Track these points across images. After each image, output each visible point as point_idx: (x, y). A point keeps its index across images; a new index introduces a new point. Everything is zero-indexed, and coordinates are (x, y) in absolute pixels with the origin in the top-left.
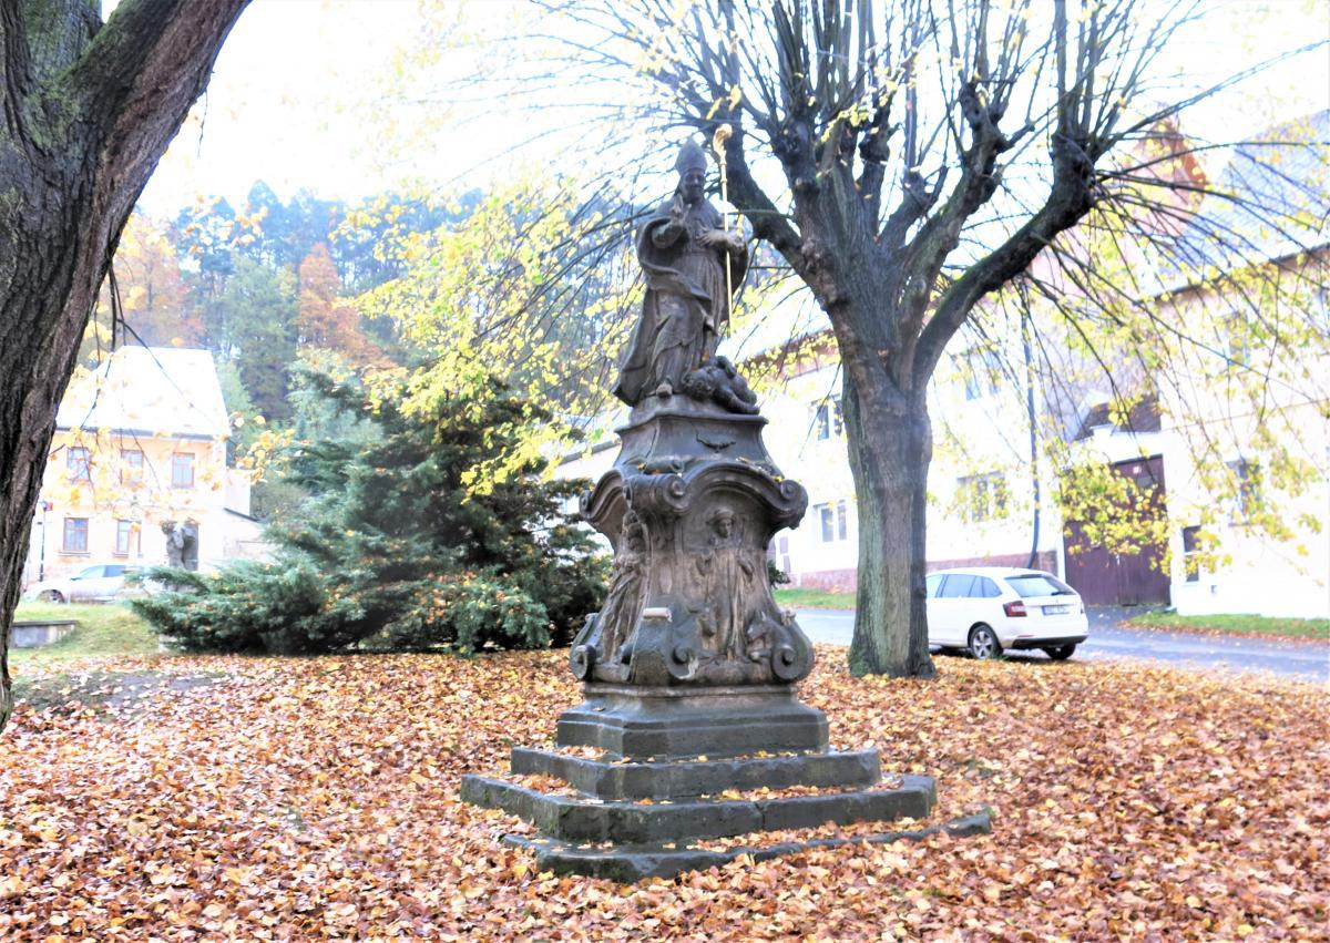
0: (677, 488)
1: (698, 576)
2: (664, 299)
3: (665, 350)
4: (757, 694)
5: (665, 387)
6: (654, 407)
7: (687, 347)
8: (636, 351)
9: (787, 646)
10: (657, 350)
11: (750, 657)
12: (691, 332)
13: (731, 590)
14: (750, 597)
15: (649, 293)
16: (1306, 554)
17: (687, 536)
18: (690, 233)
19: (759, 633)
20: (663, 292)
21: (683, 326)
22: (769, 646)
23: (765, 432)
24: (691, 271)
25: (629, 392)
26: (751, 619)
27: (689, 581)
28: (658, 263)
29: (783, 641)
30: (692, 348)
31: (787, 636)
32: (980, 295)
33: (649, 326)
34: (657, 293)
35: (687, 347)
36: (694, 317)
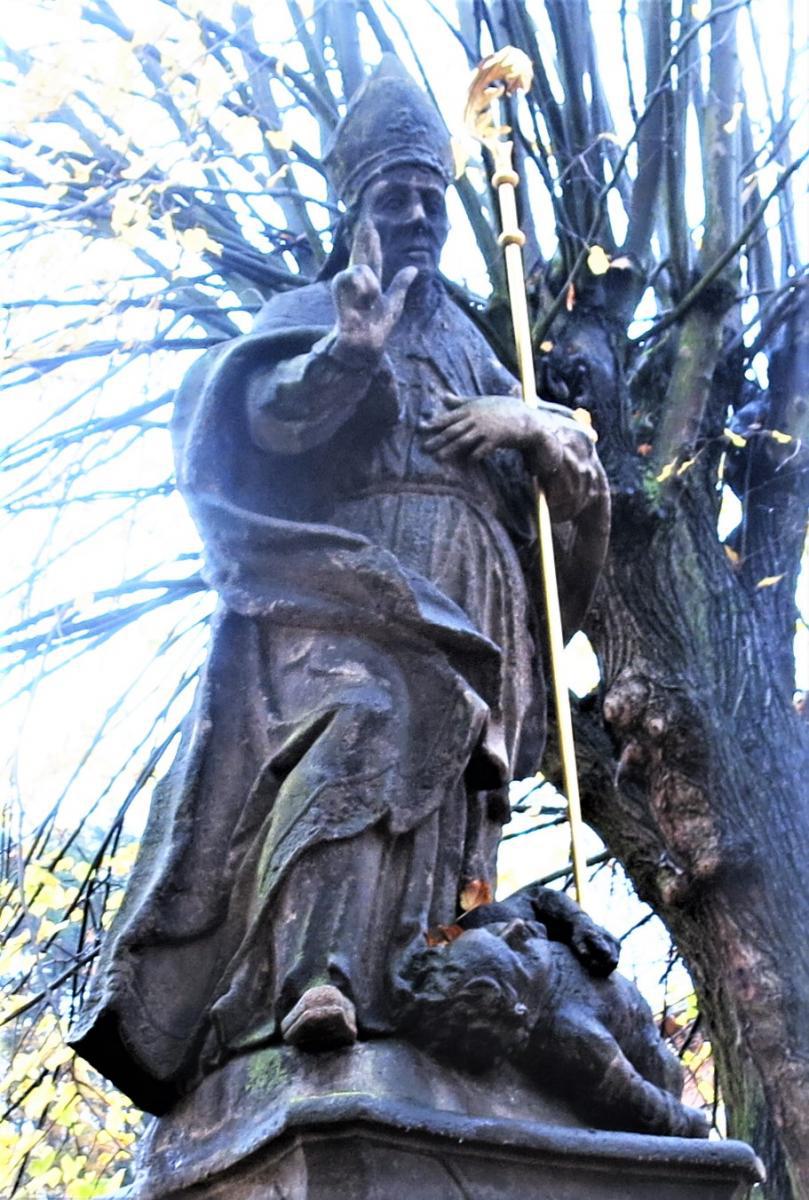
3: (316, 850)
5: (320, 998)
6: (274, 1096)
7: (406, 841)
8: (180, 864)
10: (274, 855)
12: (420, 781)
15: (232, 627)
16: (145, 387)
20: (291, 621)
21: (389, 750)
24: (350, 510)
25: (151, 1042)
30: (428, 846)
33: (231, 766)
35: (406, 841)
36: (436, 716)
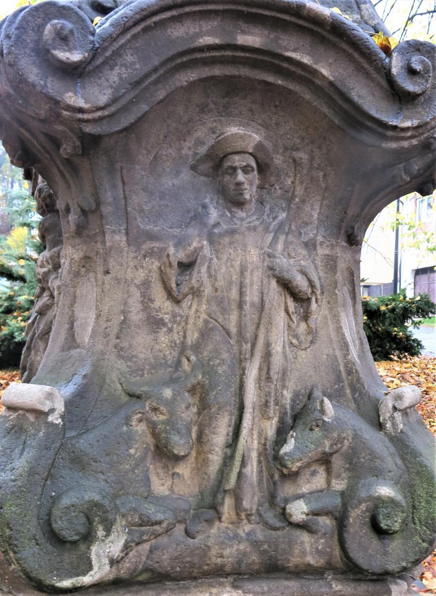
0: (63, 39)
9: (385, 491)
11: (284, 515)
13: (247, 340)
14: (304, 356)
17: (138, 199)
19: (313, 452)
22: (339, 485)
23: (361, 263)
26: (299, 416)
27: (136, 316)
29: (378, 473)
31: (390, 461)
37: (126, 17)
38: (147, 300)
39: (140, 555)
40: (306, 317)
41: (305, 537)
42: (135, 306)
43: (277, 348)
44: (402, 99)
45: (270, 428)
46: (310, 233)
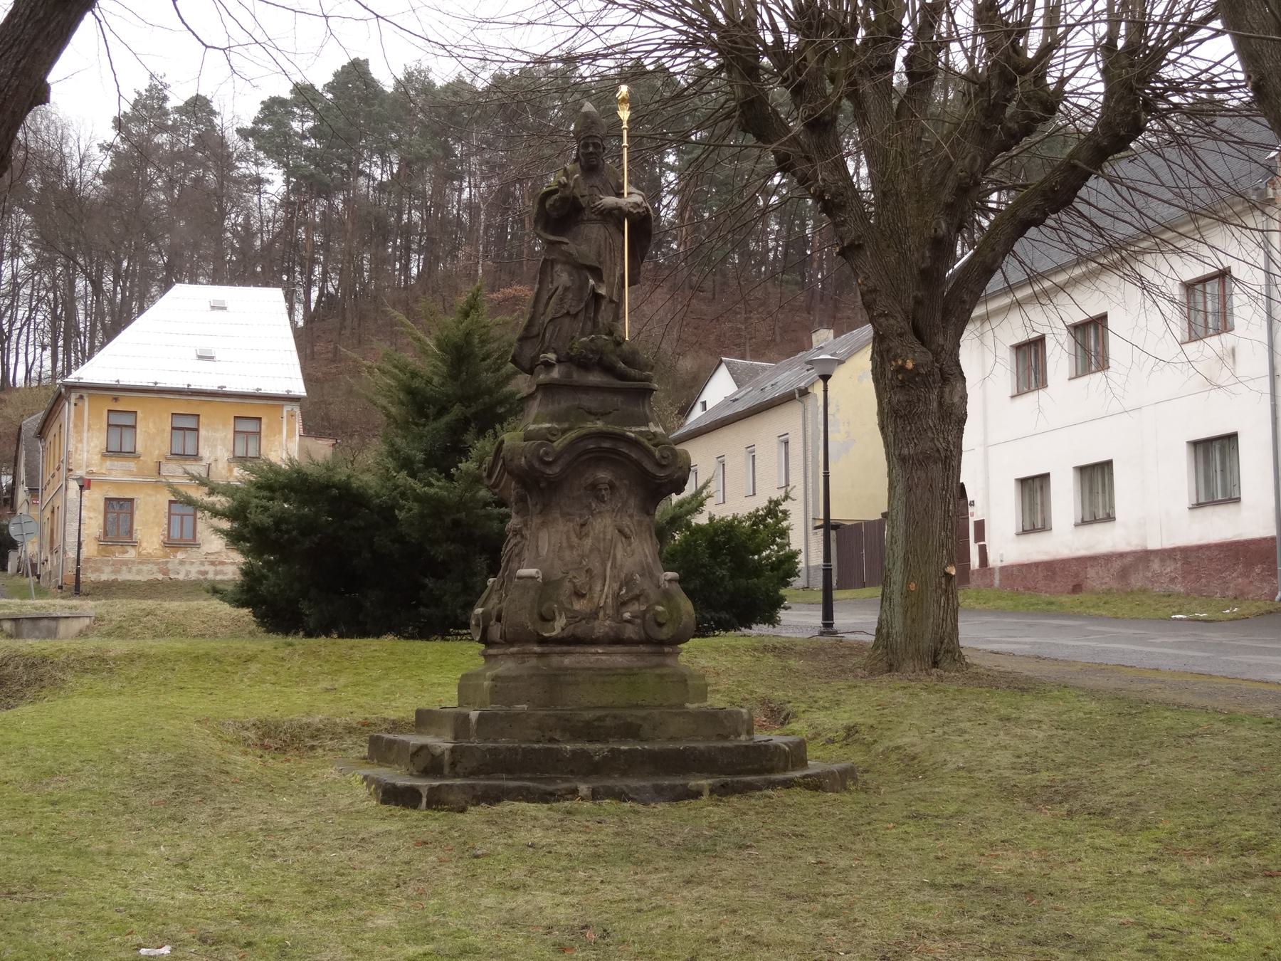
1: (575, 540)
2: (558, 267)
4: (630, 653)
18: (583, 202)
27: (565, 544)
28: (554, 234)
32: (1021, 232)
34: (553, 262)
37: (594, 487)
38: (568, 538)
39: (570, 630)
40: (630, 545)
41: (630, 626)
42: (564, 541)
43: (619, 556)
44: (663, 467)
45: (616, 586)
46: (631, 511)
